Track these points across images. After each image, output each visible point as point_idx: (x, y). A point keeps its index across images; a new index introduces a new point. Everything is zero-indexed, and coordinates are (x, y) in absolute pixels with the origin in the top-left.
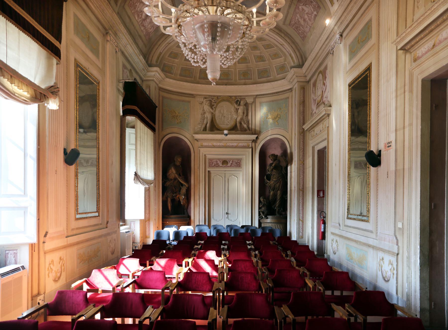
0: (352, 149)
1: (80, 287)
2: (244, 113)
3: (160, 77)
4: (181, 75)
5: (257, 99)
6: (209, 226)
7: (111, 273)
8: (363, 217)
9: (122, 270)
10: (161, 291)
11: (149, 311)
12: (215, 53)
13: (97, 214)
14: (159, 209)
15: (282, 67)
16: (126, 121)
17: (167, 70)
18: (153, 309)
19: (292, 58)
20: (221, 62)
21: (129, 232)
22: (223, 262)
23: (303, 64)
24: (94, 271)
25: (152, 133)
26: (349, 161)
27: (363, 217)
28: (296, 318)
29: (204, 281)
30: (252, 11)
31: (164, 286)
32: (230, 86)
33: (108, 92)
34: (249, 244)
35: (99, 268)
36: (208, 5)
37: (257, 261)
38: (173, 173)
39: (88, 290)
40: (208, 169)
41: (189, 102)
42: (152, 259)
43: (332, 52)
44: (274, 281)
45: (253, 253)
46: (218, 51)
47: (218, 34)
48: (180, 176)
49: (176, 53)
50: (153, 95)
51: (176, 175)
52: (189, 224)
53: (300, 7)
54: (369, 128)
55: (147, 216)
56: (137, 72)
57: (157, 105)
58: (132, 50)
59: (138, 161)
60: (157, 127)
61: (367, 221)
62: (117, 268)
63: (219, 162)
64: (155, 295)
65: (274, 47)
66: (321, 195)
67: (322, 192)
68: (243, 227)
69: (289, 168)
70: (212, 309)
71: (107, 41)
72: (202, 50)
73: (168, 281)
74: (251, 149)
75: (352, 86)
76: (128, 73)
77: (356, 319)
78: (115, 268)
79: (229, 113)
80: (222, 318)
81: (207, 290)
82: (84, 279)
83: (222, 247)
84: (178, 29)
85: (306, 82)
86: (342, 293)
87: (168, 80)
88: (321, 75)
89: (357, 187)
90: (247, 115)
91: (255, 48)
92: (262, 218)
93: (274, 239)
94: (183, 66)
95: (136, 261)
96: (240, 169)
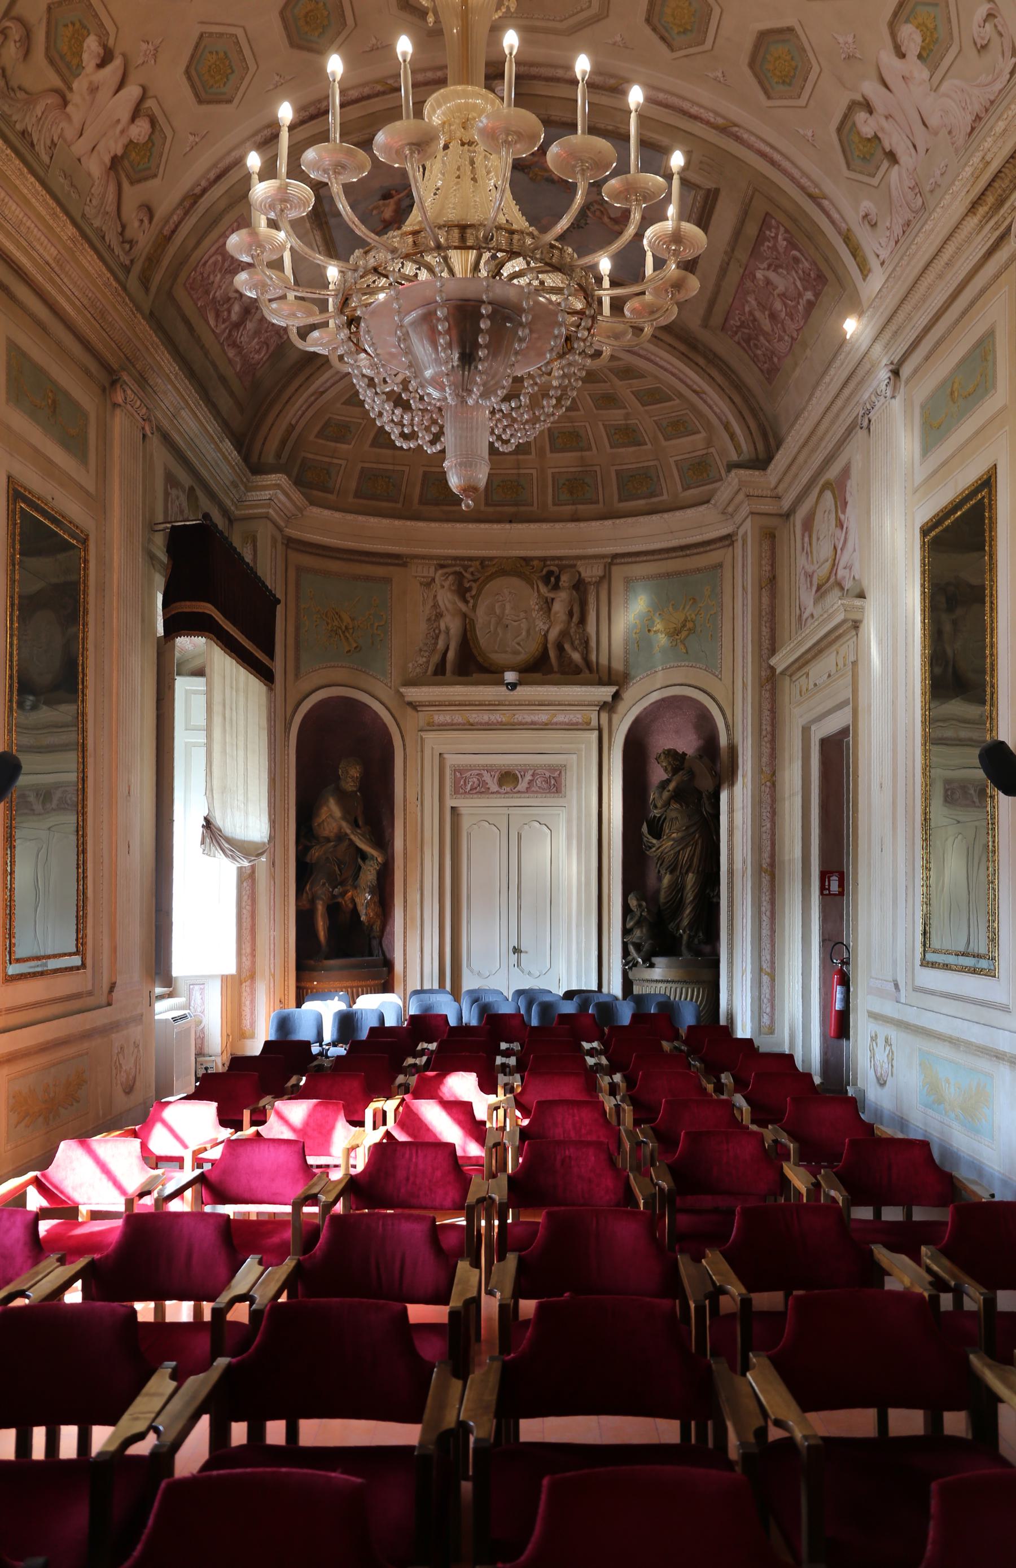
0: (935, 739)
1: (19, 1198)
2: (571, 614)
3: (288, 504)
4: (357, 495)
5: (614, 568)
6: (456, 993)
7: (120, 1152)
8: (980, 962)
9: (160, 1142)
10: (288, 1209)
11: (249, 1273)
12: (470, 402)
13: (76, 961)
14: (286, 941)
15: (699, 464)
16: (177, 654)
17: (312, 482)
18: (261, 1268)
19: (732, 436)
20: (492, 433)
21: (184, 1017)
22: (501, 1112)
23: (770, 458)
24: (63, 1145)
25: (264, 688)
26: (924, 774)
27: (980, 962)
28: (755, 1296)
29: (438, 1174)
30: (594, 268)
31: (300, 1191)
32: (525, 526)
33: (116, 565)
34: (592, 1053)
35: (83, 1137)
36: (449, 248)
37: (617, 1106)
38: (332, 815)
39: (42, 1209)
40: (450, 802)
41: (387, 580)
42: (262, 1103)
43: (865, 424)
44: (675, 1172)
45: (604, 1081)
46: (481, 396)
47: (482, 326)
48: (357, 826)
49: (346, 418)
50: (268, 566)
51: (344, 824)
52: (387, 987)
53: (759, 275)
54: (992, 670)
55: (247, 963)
56: (212, 496)
57: (279, 595)
58: (195, 425)
59: (216, 782)
60: (278, 667)
61: (990, 973)
62: (142, 1136)
63: (487, 777)
64: (273, 1223)
65: (671, 399)
66: (834, 887)
67: (836, 876)
68: (569, 995)
69: (724, 796)
70: (463, 1266)
71: (116, 405)
72: (429, 394)
73: (315, 1174)
74: (595, 734)
75: (933, 533)
76: (183, 498)
77: (958, 1302)
78: (135, 1134)
79: (522, 615)
80: (498, 1294)
81: (448, 1202)
82: (31, 1174)
83: (499, 1060)
84: (346, 331)
85: (781, 515)
86: (909, 1214)
87: (316, 510)
88: (828, 495)
89: (953, 866)
90: (583, 621)
91: (609, 401)
92: (636, 964)
93: (675, 1035)
94: (366, 465)
95: (209, 1109)
96: (560, 801)
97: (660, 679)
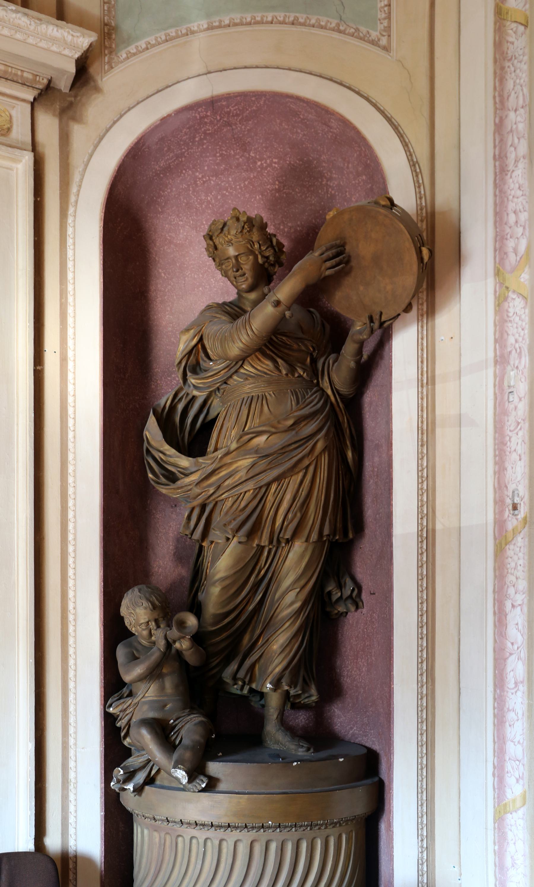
69: (404, 344)
97: (199, 49)
